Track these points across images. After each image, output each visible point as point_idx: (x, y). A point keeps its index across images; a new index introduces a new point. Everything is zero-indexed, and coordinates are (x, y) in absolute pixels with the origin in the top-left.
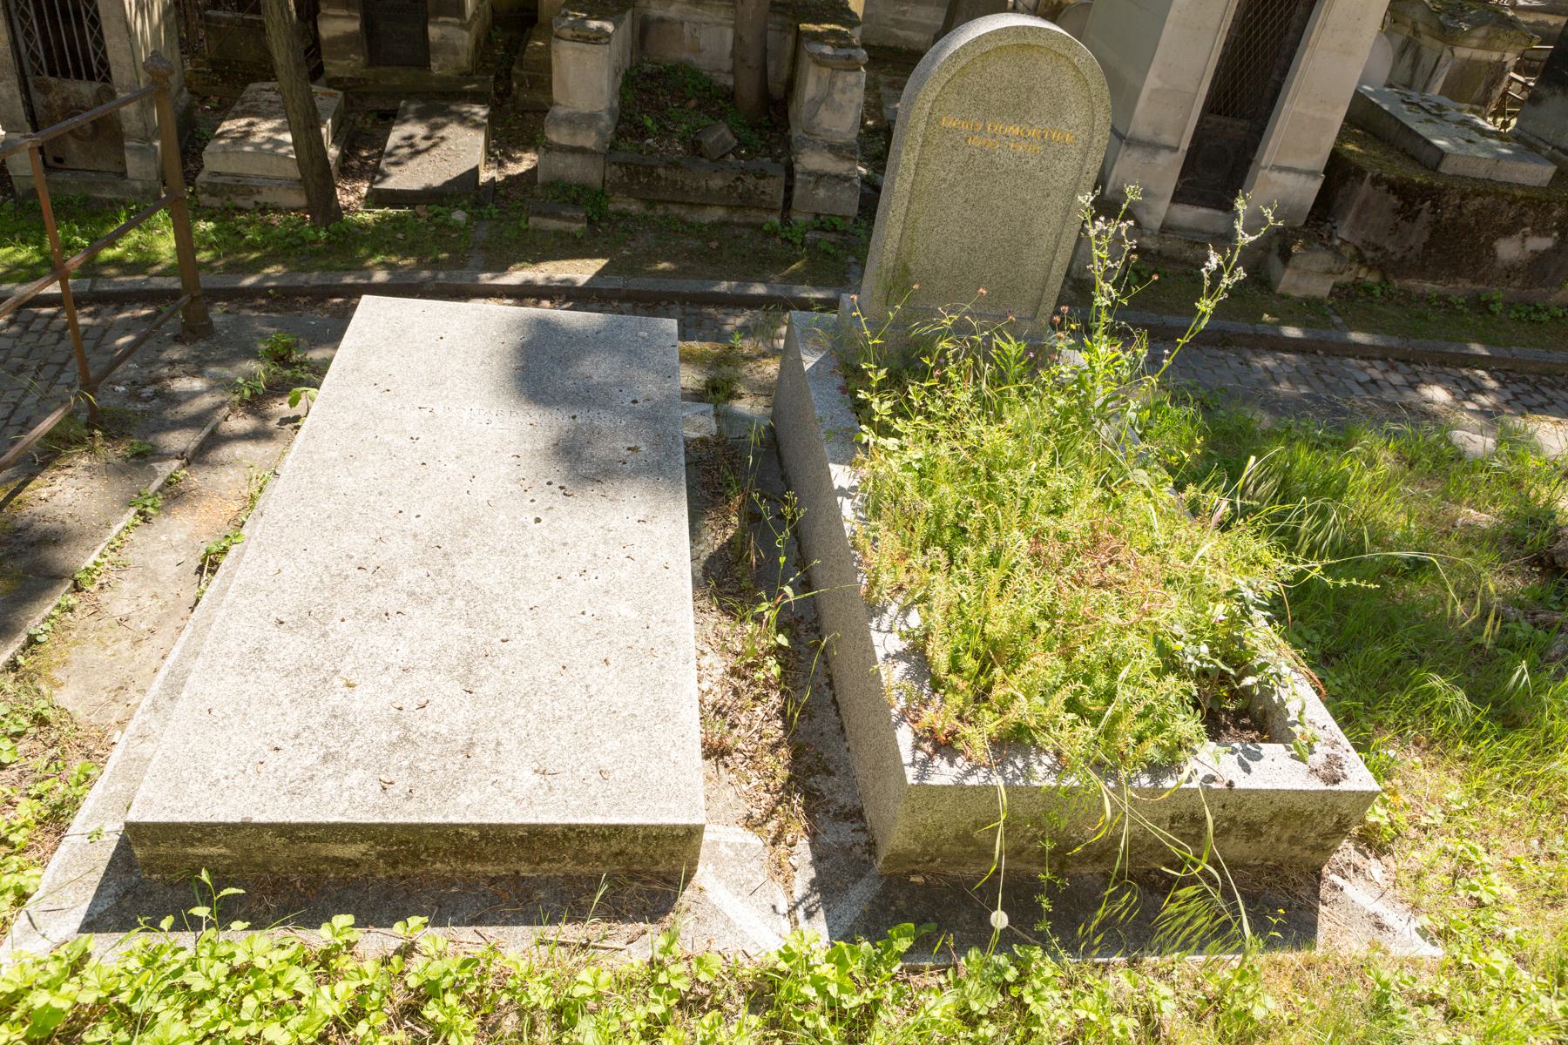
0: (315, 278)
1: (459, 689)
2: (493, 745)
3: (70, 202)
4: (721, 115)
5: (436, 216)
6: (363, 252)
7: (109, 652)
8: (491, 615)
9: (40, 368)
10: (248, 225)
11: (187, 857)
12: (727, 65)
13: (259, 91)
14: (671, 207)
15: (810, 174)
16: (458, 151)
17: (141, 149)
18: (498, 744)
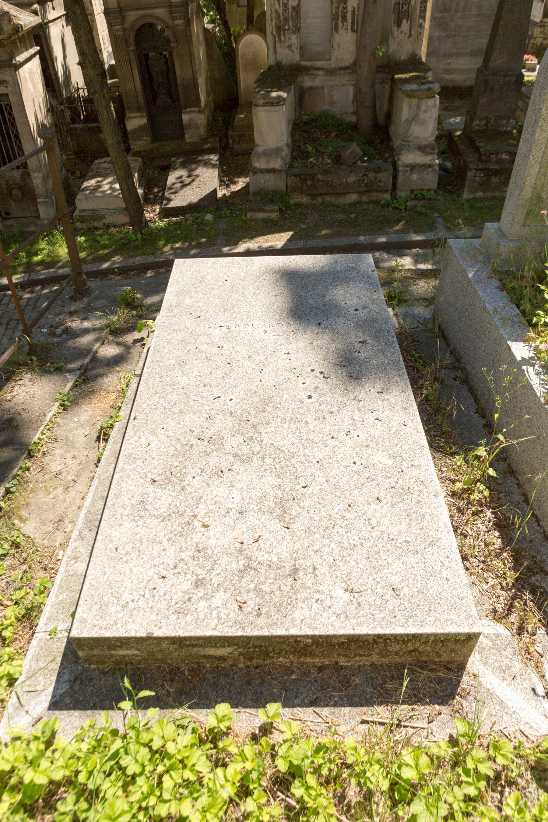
0: (138, 260)
1: (279, 526)
2: (311, 570)
3: (15, 235)
4: (351, 139)
5: (197, 219)
6: (161, 243)
7: (51, 496)
8: (291, 468)
9: (8, 324)
10: (101, 236)
11: (112, 656)
12: (351, 109)
13: (101, 163)
14: (326, 197)
15: (407, 166)
16: (204, 182)
17: (45, 202)
18: (315, 569)
